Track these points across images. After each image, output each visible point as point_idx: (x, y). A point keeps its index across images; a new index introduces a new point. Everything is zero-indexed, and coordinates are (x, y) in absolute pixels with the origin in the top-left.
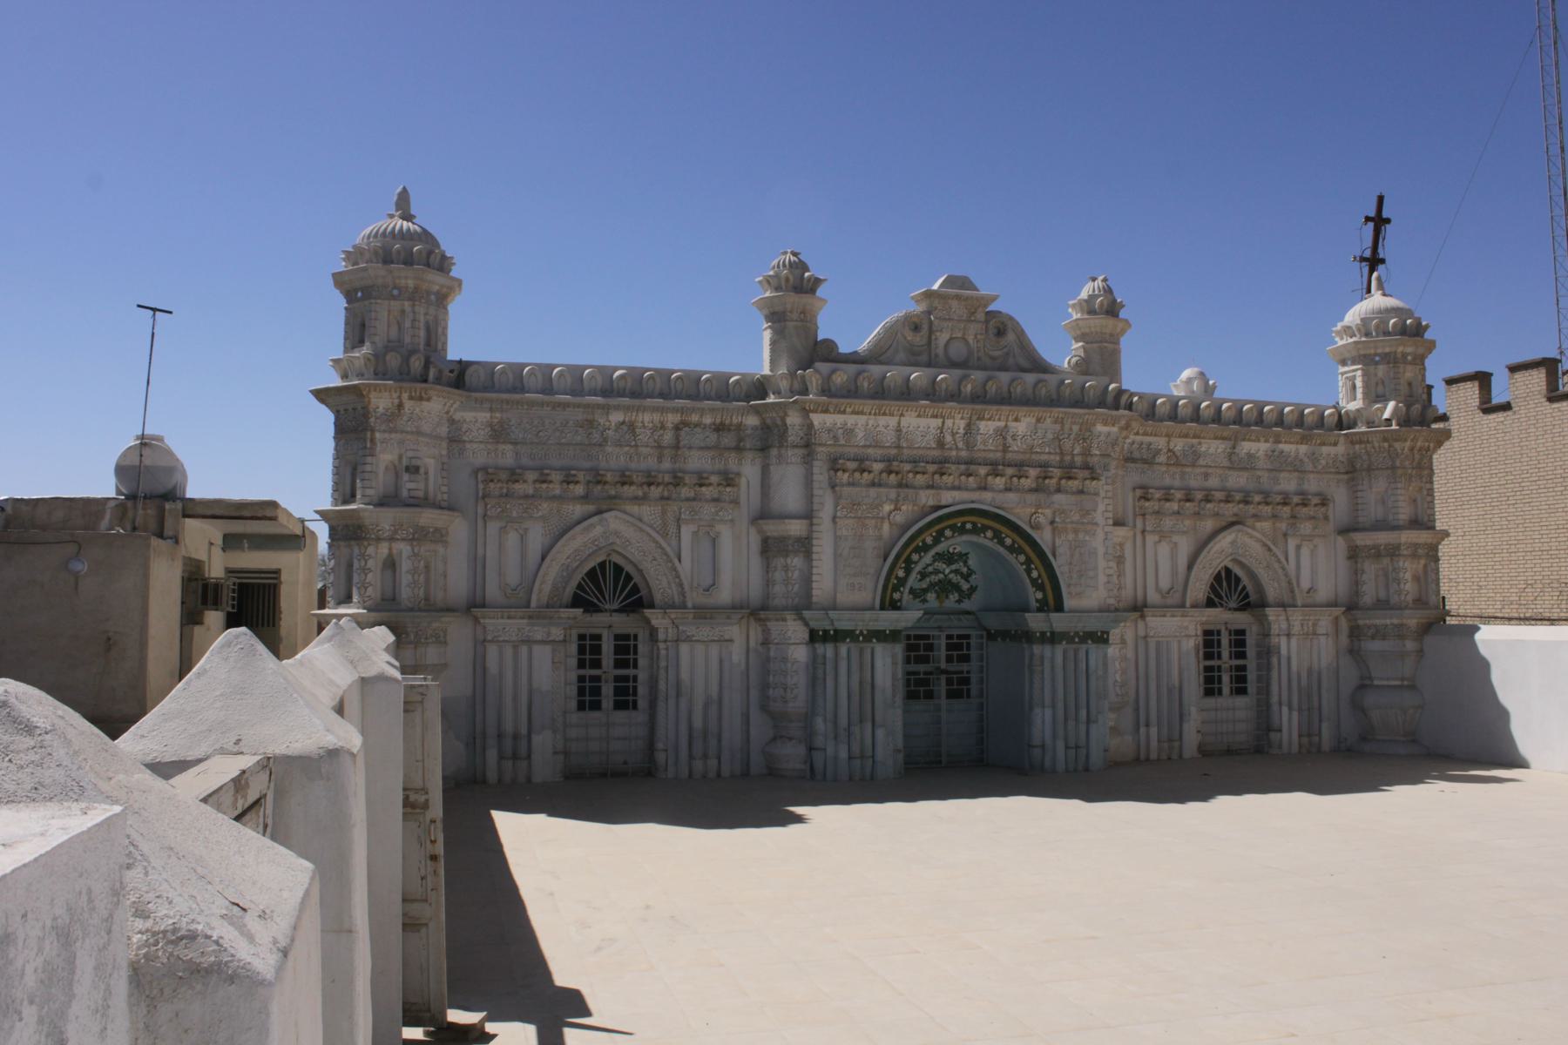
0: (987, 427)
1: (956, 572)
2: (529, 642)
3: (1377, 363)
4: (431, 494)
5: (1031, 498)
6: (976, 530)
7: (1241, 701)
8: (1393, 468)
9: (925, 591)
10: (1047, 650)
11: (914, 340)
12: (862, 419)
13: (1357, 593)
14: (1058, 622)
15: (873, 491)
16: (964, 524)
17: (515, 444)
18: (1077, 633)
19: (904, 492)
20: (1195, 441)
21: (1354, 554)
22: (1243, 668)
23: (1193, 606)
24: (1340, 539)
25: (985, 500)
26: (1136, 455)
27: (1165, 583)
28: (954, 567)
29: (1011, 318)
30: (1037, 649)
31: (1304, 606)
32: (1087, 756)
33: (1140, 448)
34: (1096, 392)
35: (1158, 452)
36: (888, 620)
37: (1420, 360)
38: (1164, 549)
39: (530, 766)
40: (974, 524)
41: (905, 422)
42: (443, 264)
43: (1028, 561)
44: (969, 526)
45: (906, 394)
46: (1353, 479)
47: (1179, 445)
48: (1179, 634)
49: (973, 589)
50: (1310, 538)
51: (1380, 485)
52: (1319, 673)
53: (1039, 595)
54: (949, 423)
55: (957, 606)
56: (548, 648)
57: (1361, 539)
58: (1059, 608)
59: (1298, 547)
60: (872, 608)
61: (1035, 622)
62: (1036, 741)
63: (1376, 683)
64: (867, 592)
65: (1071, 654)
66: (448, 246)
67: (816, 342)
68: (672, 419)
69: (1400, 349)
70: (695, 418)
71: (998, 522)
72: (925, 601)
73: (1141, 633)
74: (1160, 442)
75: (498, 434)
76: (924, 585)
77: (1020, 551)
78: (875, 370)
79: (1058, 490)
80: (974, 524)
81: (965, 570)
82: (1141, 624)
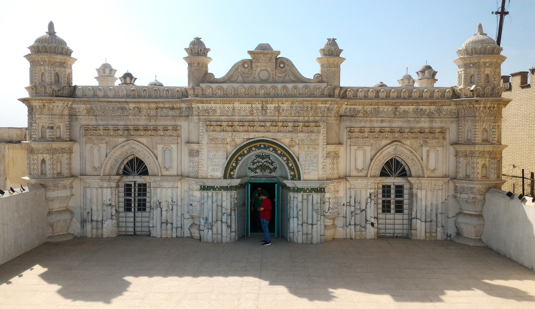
0: (271, 106)
1: (266, 162)
2: (102, 188)
3: (470, 67)
4: (62, 137)
5: (289, 135)
6: (265, 148)
7: (399, 216)
8: (475, 116)
9: (256, 169)
10: (296, 195)
11: (242, 71)
12: (218, 105)
13: (457, 172)
14: (299, 184)
15: (222, 134)
16: (260, 145)
17: (96, 116)
18: (308, 189)
19: (234, 134)
20: (376, 107)
21: (456, 155)
22: (402, 202)
23: (370, 177)
24: (451, 148)
25: (269, 136)
26: (348, 114)
27: (360, 166)
28: (265, 160)
29: (288, 60)
30: (291, 194)
31: (428, 177)
32: (312, 238)
33: (350, 111)
34: (328, 86)
35: (359, 112)
36: (226, 183)
37: (498, 66)
38: (360, 153)
39: (102, 231)
40: (265, 145)
41: (235, 106)
42: (68, 53)
43: (288, 160)
44: (262, 146)
45: (237, 96)
46: (458, 121)
47: (369, 108)
48: (367, 188)
49: (275, 168)
50: (435, 147)
51: (469, 125)
52: (437, 206)
53: (292, 173)
54: (254, 105)
55: (269, 174)
56: (109, 190)
57: (462, 148)
58: (299, 179)
59: (428, 151)
60: (221, 179)
61: (289, 183)
62: (291, 231)
63: (465, 212)
64: (220, 173)
65: (305, 197)
66: (70, 45)
67: (206, 73)
68: (153, 106)
69: (482, 60)
70: (161, 105)
71: (274, 145)
72: (256, 172)
73: (348, 187)
74: (360, 107)
75: (89, 112)
76: (255, 166)
77: (284, 156)
78: (225, 86)
79: (302, 132)
80: (265, 145)
81: (270, 161)
82: (348, 183)
